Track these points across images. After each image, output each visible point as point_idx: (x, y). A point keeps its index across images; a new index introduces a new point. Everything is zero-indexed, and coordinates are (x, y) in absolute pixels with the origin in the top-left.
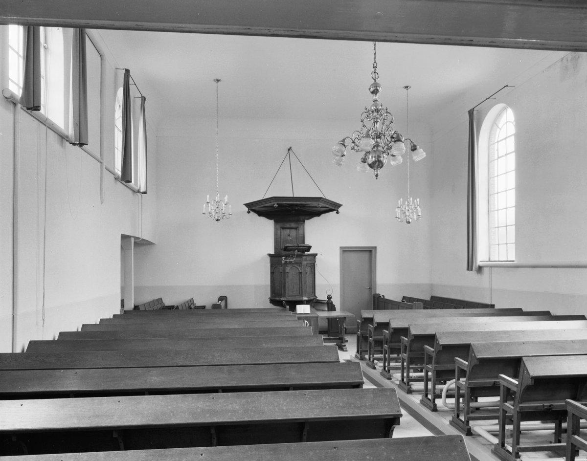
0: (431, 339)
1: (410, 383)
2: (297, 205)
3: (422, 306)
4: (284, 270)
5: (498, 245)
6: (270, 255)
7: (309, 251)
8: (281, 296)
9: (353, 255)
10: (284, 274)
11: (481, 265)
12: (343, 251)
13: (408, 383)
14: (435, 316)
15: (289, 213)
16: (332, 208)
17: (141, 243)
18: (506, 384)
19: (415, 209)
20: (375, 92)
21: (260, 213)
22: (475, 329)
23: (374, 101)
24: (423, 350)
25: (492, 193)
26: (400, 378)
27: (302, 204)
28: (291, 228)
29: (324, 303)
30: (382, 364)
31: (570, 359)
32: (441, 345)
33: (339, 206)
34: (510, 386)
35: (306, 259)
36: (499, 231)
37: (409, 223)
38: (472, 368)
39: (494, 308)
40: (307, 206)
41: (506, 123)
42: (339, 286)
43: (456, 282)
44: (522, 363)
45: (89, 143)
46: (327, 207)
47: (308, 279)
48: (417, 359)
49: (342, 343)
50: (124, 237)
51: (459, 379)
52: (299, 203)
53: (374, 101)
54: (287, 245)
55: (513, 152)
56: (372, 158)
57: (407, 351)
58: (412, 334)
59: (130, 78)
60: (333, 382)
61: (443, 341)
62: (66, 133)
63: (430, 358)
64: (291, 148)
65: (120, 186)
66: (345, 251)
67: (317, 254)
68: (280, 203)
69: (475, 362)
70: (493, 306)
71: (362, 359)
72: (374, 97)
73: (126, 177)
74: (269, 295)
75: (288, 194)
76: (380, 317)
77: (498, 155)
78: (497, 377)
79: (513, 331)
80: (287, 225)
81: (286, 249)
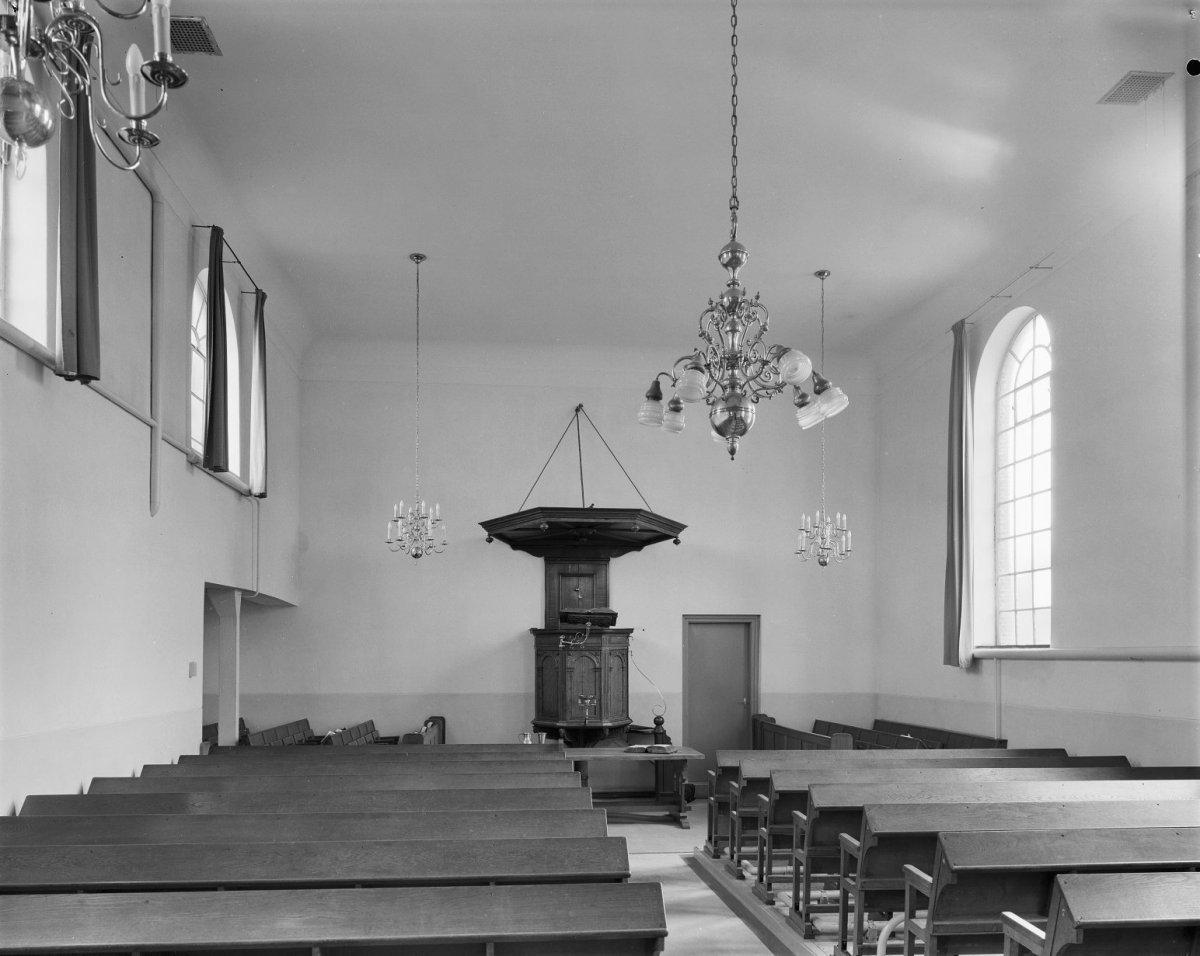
0: (852, 817)
1: (812, 915)
2: (591, 526)
3: (851, 743)
4: (564, 661)
5: (1016, 611)
6: (534, 631)
7: (614, 625)
8: (557, 718)
9: (712, 633)
10: (563, 673)
11: (976, 655)
12: (690, 623)
13: (807, 915)
14: (870, 765)
15: (575, 543)
16: (663, 531)
17: (256, 604)
18: (1017, 937)
19: (839, 530)
20: (734, 263)
21: (516, 544)
22: (957, 798)
23: (729, 285)
24: (837, 842)
25: (1003, 501)
26: (791, 903)
27: (601, 524)
28: (579, 575)
29: (648, 734)
30: (755, 870)
31: (1168, 879)
32: (876, 835)
33: (681, 527)
34: (1026, 944)
35: (610, 641)
36: (1016, 588)
37: (824, 564)
38: (942, 893)
39: (1006, 747)
40: (612, 527)
41: (1033, 349)
42: (681, 697)
43: (927, 692)
44: (1055, 889)
45: (102, 377)
46: (655, 531)
47: (612, 679)
48: (825, 860)
49: (680, 811)
50: (212, 592)
51: (912, 915)
52: (592, 521)
53: (729, 285)
54: (566, 610)
55: (1045, 412)
56: (723, 411)
57: (805, 844)
58: (816, 805)
59: (225, 246)
60: (592, 931)
61: (881, 824)
62: (49, 352)
63: (852, 860)
64: (581, 406)
65: (202, 478)
66: (692, 622)
67: (631, 630)
68: (553, 520)
69: (947, 879)
70: (1002, 743)
71: (717, 855)
72: (729, 274)
73: (213, 459)
74: (533, 716)
75: (575, 502)
76: (754, 765)
77: (1015, 420)
78: (998, 914)
79: (1042, 805)
80: (571, 568)
81: (565, 618)
